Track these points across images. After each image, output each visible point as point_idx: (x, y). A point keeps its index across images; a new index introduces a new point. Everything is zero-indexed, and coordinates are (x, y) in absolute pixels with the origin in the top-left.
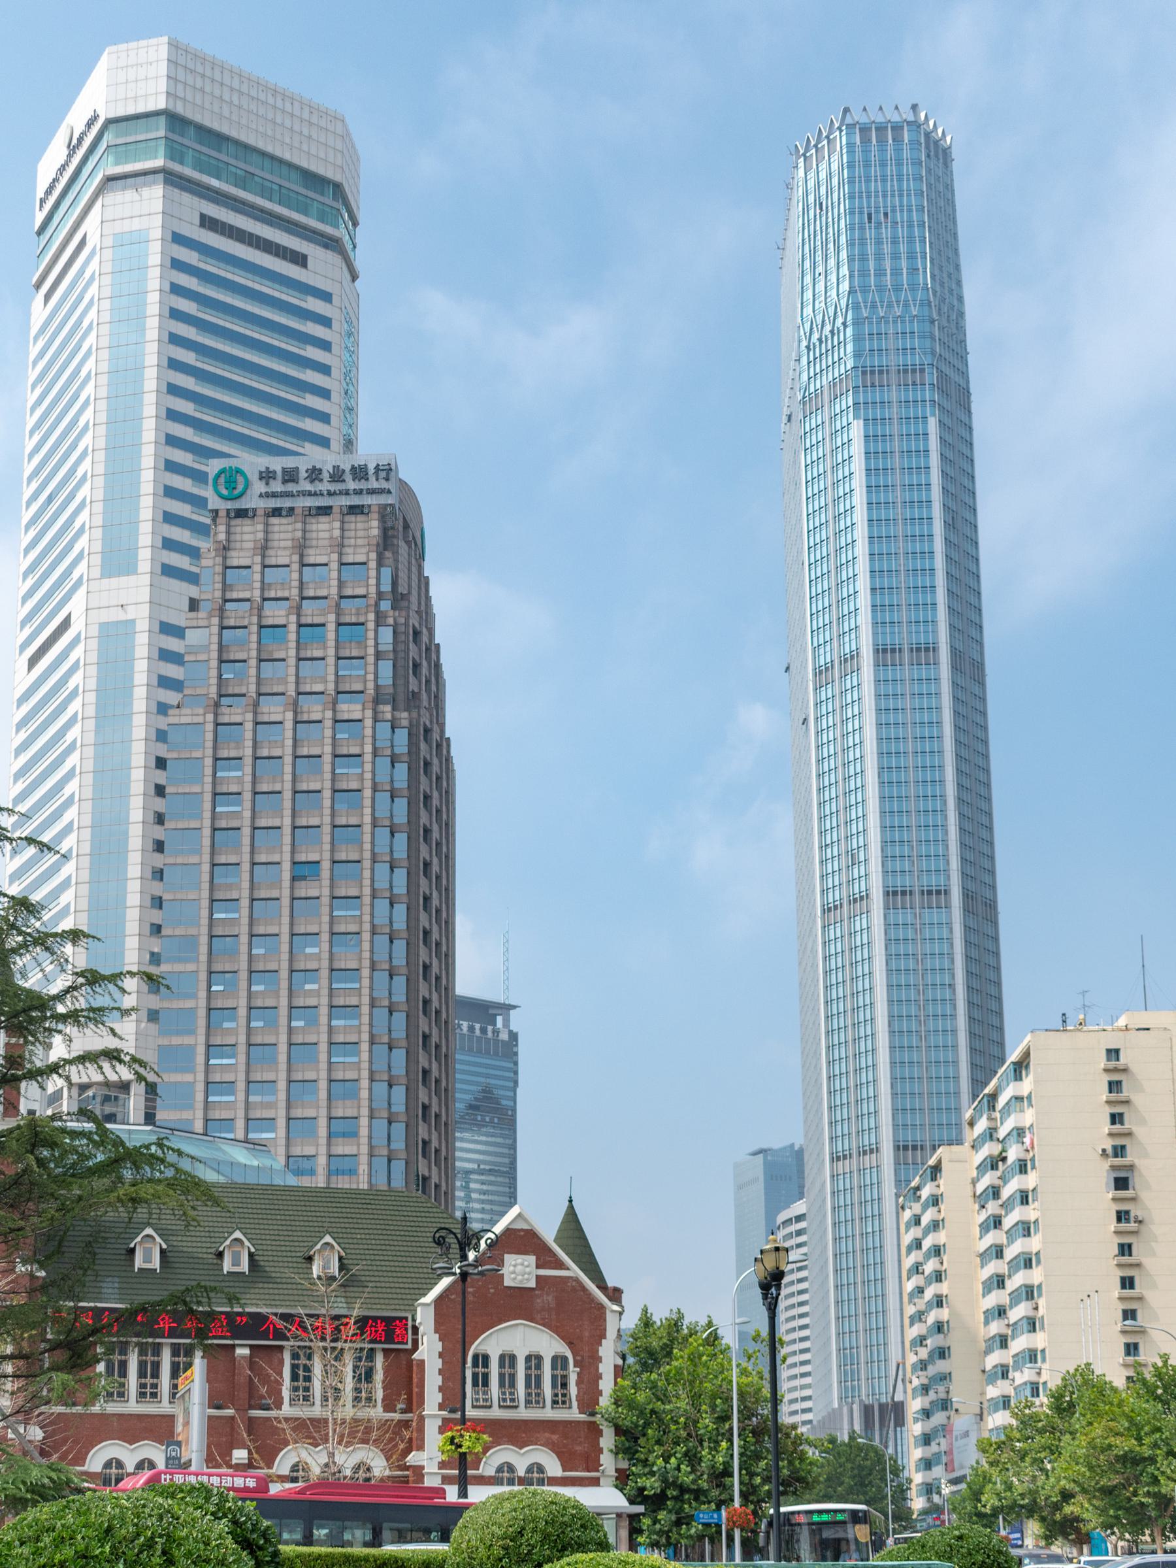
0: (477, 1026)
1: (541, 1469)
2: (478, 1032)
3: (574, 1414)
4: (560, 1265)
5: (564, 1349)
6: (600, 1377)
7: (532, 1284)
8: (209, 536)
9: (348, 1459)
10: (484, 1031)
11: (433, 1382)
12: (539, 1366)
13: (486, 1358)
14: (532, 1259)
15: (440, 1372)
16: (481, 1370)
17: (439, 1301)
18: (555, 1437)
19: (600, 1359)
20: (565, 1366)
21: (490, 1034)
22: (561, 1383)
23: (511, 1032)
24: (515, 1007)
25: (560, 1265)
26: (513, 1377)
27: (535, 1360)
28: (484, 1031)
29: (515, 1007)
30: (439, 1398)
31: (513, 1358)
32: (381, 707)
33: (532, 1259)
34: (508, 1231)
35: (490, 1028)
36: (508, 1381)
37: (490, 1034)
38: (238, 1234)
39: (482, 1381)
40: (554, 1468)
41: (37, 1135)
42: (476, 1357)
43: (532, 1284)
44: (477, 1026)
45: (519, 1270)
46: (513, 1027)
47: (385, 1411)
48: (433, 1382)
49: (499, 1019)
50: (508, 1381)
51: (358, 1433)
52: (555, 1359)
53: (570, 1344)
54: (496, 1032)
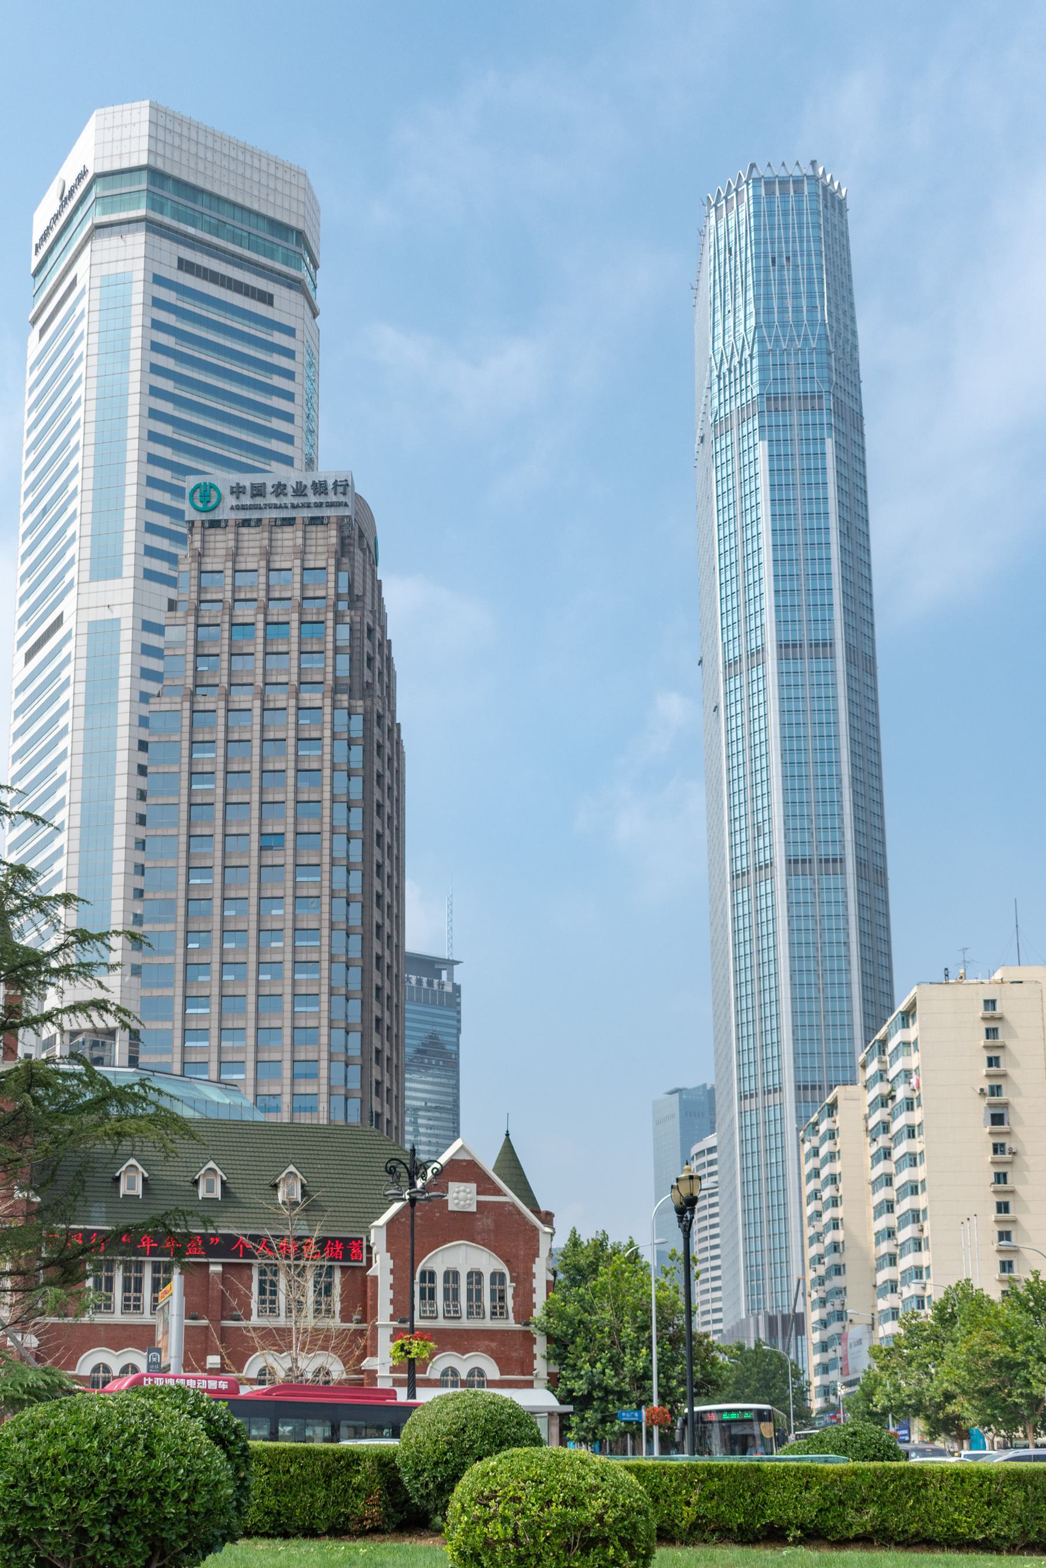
0: (425, 980)
1: (481, 1373)
2: (425, 985)
3: (510, 1324)
4: (498, 1192)
5: (501, 1267)
6: (534, 1291)
7: (473, 1208)
8: (186, 544)
9: (309, 1364)
10: (430, 983)
11: (385, 1295)
12: (479, 1282)
13: (432, 1274)
14: (473, 1186)
15: (392, 1287)
16: (427, 1285)
17: (391, 1224)
18: (493, 1345)
19: (533, 1276)
20: (502, 1282)
21: (436, 987)
22: (499, 1297)
23: (454, 985)
24: (458, 963)
25: (498, 1192)
26: (456, 1291)
27: (475, 1276)
28: (430, 983)
29: (458, 963)
30: (390, 1310)
31: (456, 1274)
32: (339, 696)
33: (473, 1186)
34: (452, 1162)
35: (436, 981)
36: (452, 1295)
37: (436, 987)
38: (211, 1165)
39: (429, 1295)
40: (493, 1372)
41: (33, 1076)
42: (423, 1273)
43: (473, 1208)
44: (425, 980)
45: (461, 1196)
46: (457, 981)
47: (342, 1321)
48: (385, 1295)
49: (444, 973)
50: (452, 1295)
51: (318, 1341)
52: (493, 1275)
53: (507, 1262)
54: (441, 985)
